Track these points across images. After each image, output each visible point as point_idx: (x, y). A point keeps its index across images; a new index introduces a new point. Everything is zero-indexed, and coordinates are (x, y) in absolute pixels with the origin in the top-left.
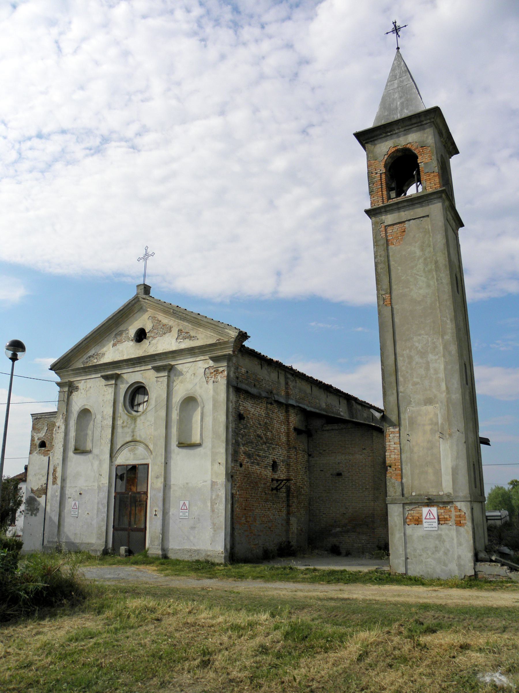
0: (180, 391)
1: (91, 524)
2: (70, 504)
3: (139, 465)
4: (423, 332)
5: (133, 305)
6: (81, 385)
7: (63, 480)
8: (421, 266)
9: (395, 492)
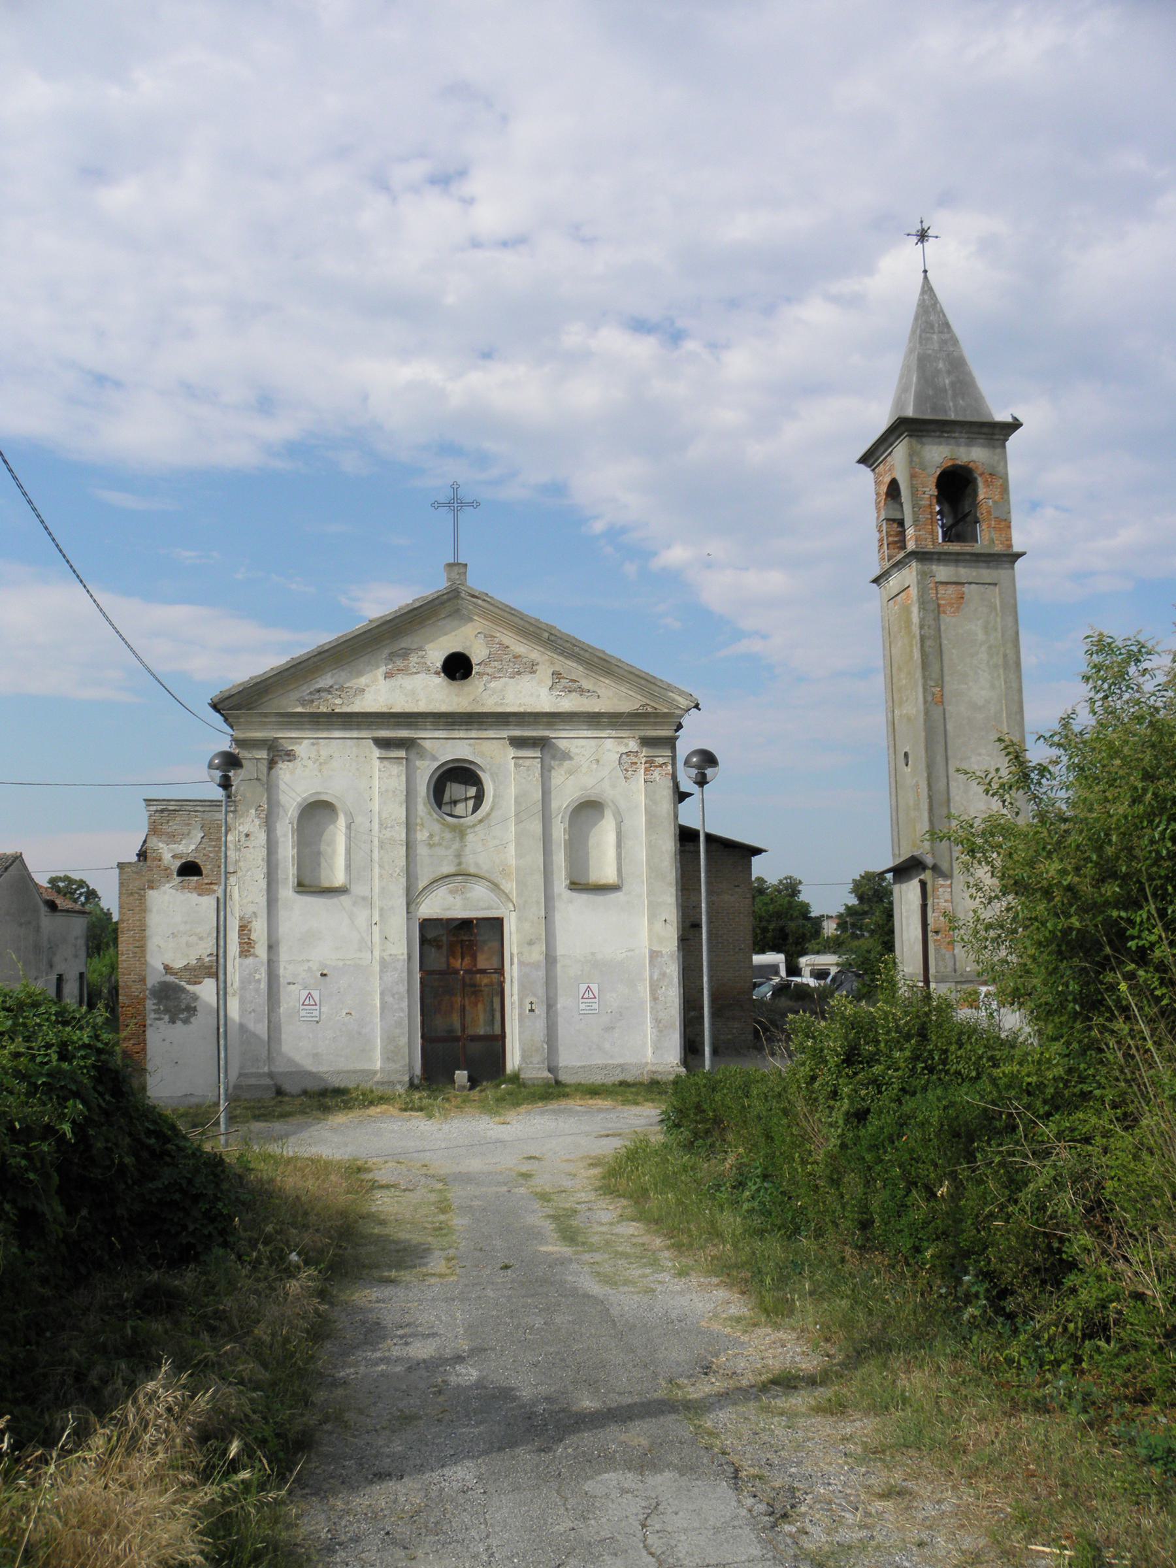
0: (568, 789)
1: (360, 1033)
2: (292, 996)
3: (477, 919)
4: (983, 751)
5: (442, 603)
6: (303, 749)
7: (272, 947)
8: (984, 656)
9: (946, 967)
